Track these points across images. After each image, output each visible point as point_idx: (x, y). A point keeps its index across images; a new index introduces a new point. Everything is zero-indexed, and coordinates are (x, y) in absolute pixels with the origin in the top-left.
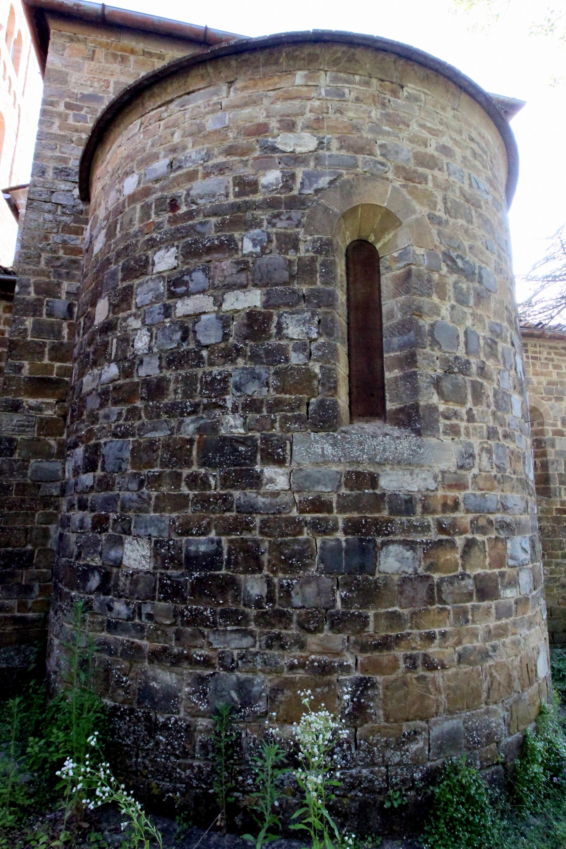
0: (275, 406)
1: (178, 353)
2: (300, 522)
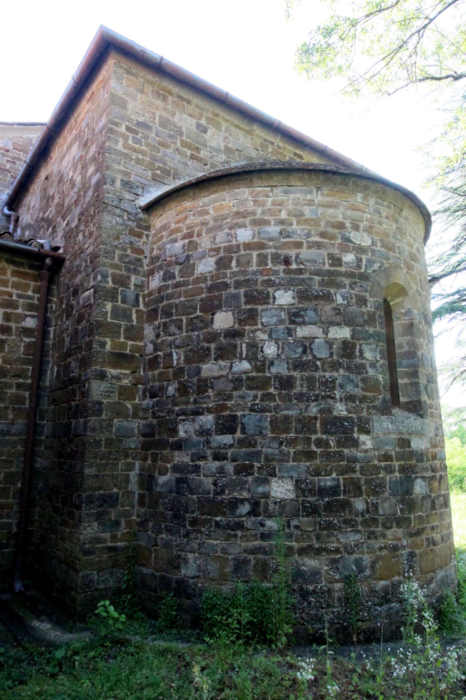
0: (363, 399)
1: (301, 361)
2: (379, 467)
